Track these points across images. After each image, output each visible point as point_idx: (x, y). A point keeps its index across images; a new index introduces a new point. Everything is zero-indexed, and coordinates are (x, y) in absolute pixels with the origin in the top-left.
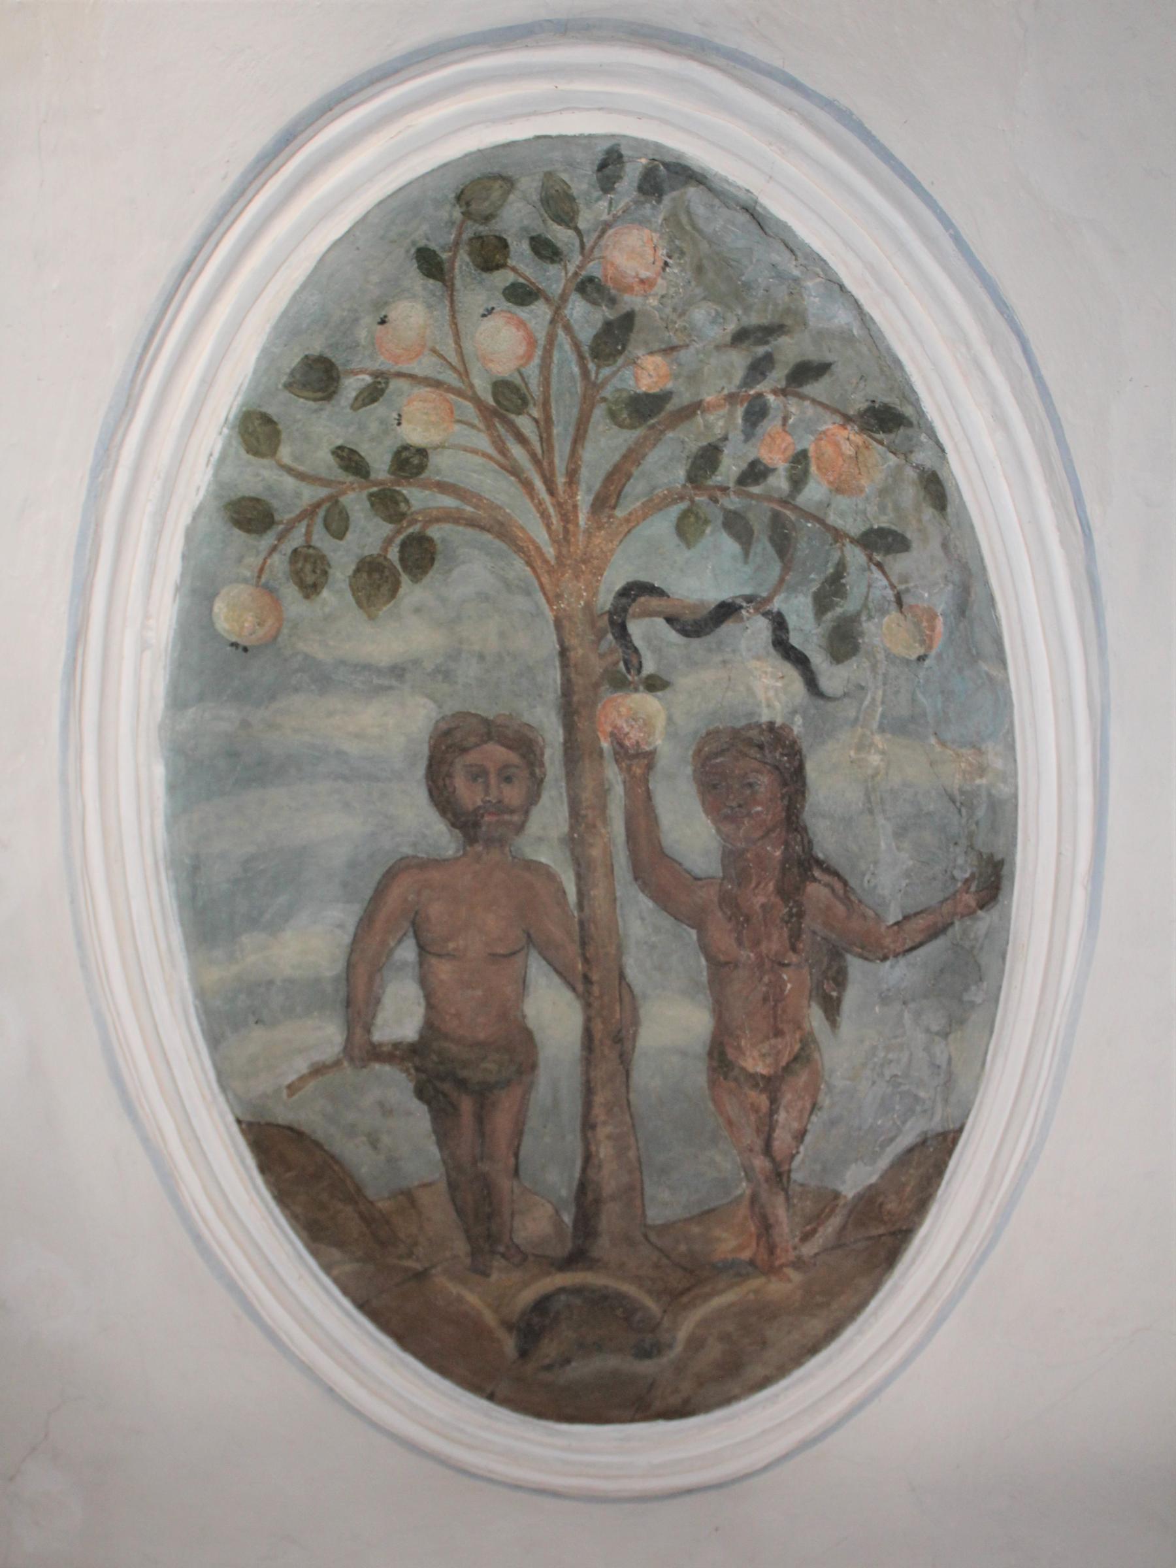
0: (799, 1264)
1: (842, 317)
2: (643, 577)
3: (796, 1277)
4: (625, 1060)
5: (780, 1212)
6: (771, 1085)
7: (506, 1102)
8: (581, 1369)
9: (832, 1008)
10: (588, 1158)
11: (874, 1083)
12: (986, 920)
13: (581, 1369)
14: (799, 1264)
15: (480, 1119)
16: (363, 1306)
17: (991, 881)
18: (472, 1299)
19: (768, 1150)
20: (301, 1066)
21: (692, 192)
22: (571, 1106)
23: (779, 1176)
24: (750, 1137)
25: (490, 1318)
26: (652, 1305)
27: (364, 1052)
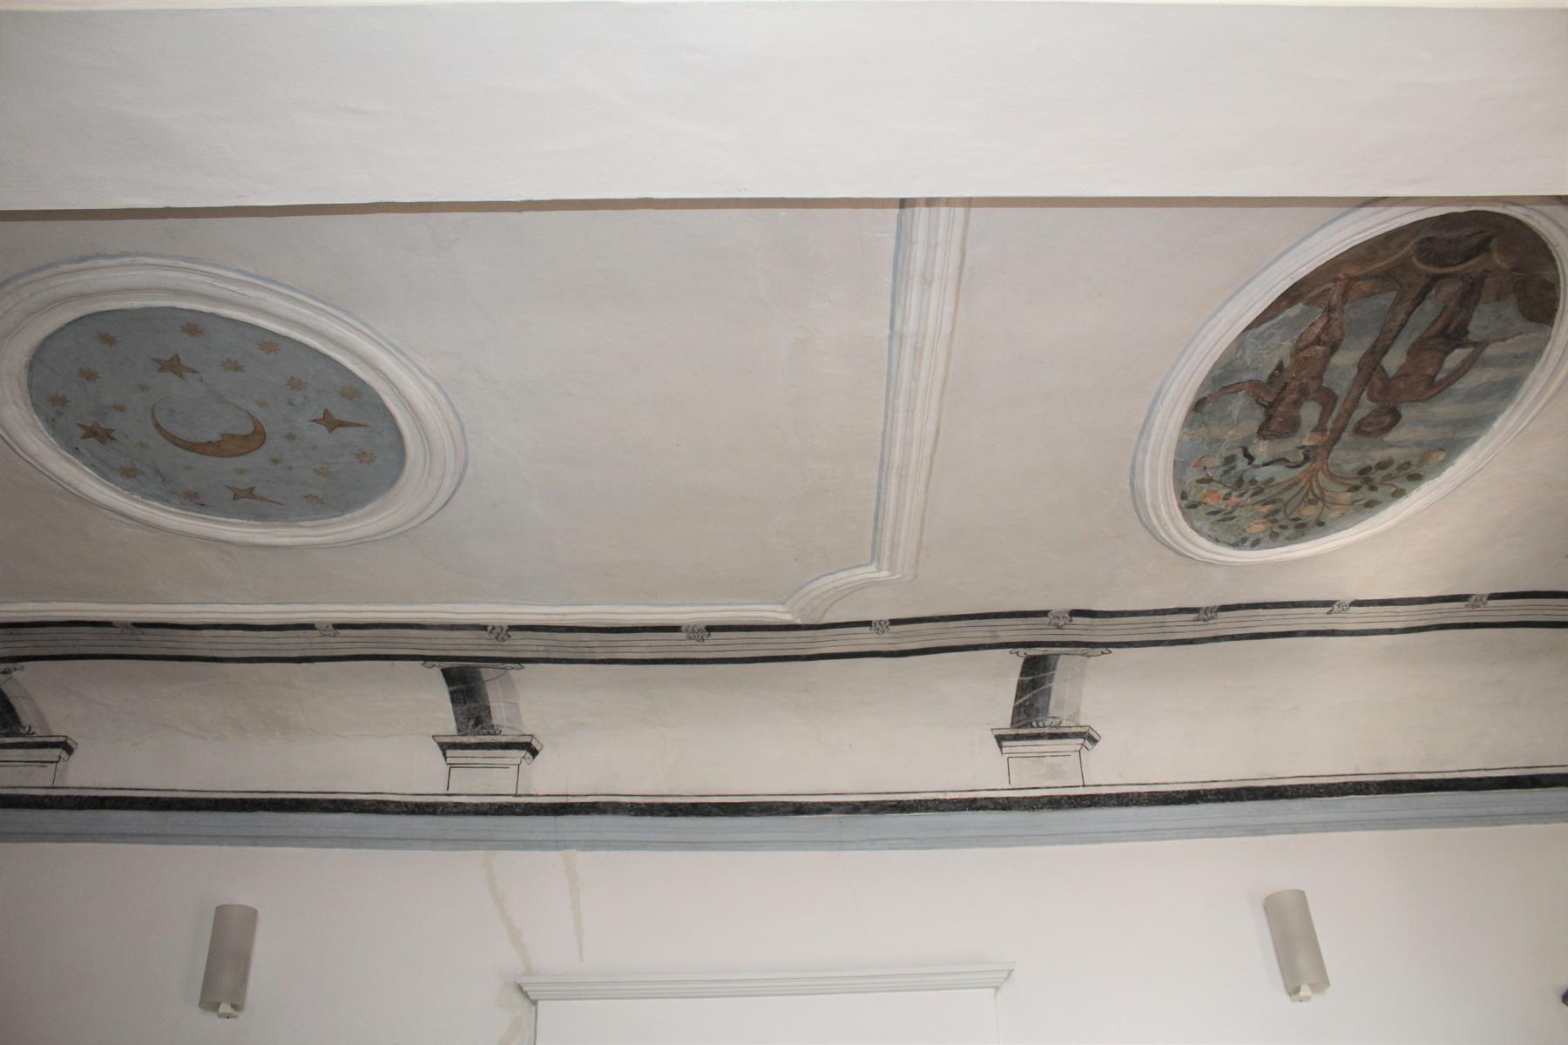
0: (1336, 280)
1: (1198, 524)
2: (264, 447)
3: (1341, 275)
4: (1374, 346)
5: (1335, 299)
6: (1318, 341)
7: (1433, 331)
8: (1468, 231)
9: (1280, 367)
10: (1409, 314)
11: (1209, 480)
12: (1206, 394)
13: (1468, 231)
14: (1336, 280)
15: (1447, 326)
16: (1552, 259)
17: (1198, 406)
18: (1498, 261)
19: (1330, 319)
20: (1509, 341)
21: (1233, 540)
22: (1405, 332)
23: (1330, 310)
24: (1334, 324)
25: (1495, 254)
26: (1414, 260)
27: (1480, 345)
